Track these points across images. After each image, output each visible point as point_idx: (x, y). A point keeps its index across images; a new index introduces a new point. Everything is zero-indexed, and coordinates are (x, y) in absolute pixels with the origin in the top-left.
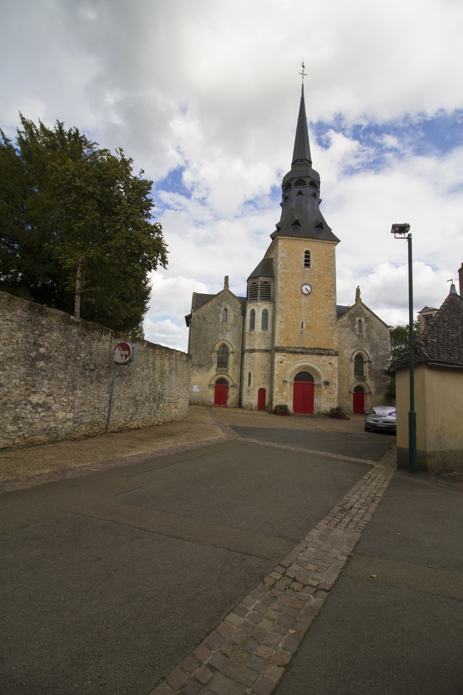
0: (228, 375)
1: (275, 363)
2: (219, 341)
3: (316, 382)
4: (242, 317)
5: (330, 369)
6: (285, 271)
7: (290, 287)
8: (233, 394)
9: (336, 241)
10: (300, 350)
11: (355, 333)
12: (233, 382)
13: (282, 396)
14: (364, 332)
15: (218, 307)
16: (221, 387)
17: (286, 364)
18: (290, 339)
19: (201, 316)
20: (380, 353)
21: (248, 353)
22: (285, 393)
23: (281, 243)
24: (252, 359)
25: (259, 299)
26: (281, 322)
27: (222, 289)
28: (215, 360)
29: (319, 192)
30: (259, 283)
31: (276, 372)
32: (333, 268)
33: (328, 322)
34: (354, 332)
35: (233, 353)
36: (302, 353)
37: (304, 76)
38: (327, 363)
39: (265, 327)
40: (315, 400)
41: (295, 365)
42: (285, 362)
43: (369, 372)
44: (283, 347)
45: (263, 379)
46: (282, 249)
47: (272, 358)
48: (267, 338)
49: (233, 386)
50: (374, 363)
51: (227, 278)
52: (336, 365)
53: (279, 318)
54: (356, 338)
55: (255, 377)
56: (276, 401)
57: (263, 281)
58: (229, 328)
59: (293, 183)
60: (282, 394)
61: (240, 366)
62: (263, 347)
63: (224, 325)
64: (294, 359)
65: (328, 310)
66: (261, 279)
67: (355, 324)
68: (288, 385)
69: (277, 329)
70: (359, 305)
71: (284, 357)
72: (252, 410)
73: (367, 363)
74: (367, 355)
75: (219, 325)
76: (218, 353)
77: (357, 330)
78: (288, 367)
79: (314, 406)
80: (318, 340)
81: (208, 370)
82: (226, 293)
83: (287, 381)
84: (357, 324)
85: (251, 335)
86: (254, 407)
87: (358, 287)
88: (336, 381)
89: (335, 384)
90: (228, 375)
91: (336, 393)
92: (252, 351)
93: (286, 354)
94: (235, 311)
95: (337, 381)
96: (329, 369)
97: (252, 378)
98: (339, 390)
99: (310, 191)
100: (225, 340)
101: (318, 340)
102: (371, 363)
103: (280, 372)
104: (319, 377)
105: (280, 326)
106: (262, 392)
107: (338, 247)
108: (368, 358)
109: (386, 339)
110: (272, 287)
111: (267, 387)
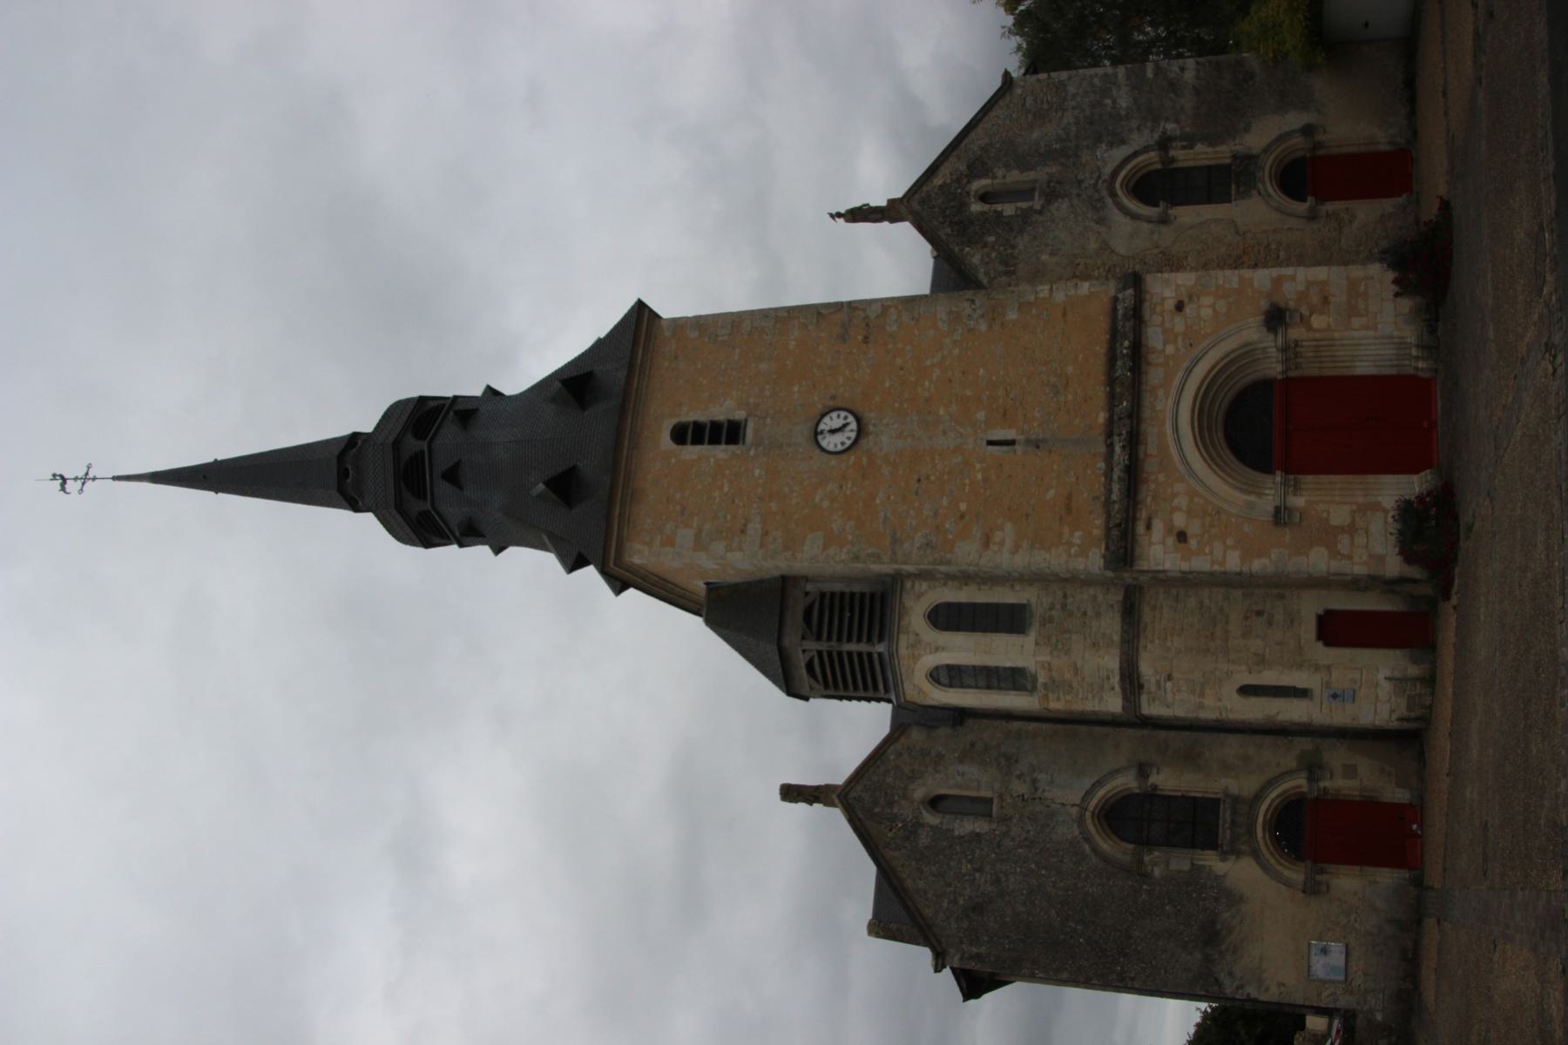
0: (1258, 797)
1: (1185, 566)
2: (1088, 839)
3: (1273, 367)
4: (970, 722)
5: (1205, 308)
6: (755, 527)
7: (826, 504)
8: (1350, 771)
9: (641, 311)
10: (1118, 449)
11: (1040, 212)
12: (1290, 773)
14: (1031, 175)
15: (924, 839)
16: (1317, 833)
17: (1190, 512)
18: (1069, 497)
19: (965, 924)
20: (1124, 103)
21: (1144, 698)
22: (1339, 515)
23: (639, 556)
24: (1169, 677)
26: (987, 542)
27: (836, 816)
28: (1180, 861)
29: (456, 398)
30: (813, 646)
31: (1233, 562)
32: (747, 325)
33: (983, 327)
34: (1035, 217)
35: (1143, 771)
36: (1134, 441)
37: (91, 475)
38: (1179, 324)
39: (1009, 620)
40: (1364, 368)
41: (1192, 473)
42: (1179, 520)
43: (1212, 140)
44: (1108, 529)
47: (1162, 580)
48: (1064, 606)
49: (1313, 768)
50: (1171, 127)
51: (791, 793)
52: (1185, 279)
53: (967, 553)
54: (1061, 208)
55: (1261, 661)
57: (805, 631)
58: (1020, 788)
59: (417, 506)
60: (1342, 529)
62: (1111, 624)
64: (1161, 477)
66: (792, 640)
67: (999, 214)
68: (1298, 501)
69: (1020, 561)
70: (915, 205)
71: (1158, 525)
72: (1430, 681)
73: (1172, 153)
74: (1135, 154)
77: (1024, 205)
78: (1206, 513)
79: (1394, 372)
80: (1070, 369)
81: (1233, 899)
82: (864, 800)
83: (1277, 510)
84: (999, 207)
85: (1053, 685)
86: (1413, 671)
88: (1262, 278)
89: (1278, 282)
90: (1258, 797)
91: (1321, 273)
92: (1131, 681)
93: (1143, 514)
95: (1266, 272)
96: (1206, 313)
97: (1270, 677)
98: (1301, 259)
99: (449, 434)
100: (1083, 809)
101: (1070, 369)
103: (1230, 542)
104: (1247, 354)
106: (1338, 630)
107: (667, 307)
108: (1146, 150)
109: (1061, 86)
110: (828, 587)
111: (1310, 607)
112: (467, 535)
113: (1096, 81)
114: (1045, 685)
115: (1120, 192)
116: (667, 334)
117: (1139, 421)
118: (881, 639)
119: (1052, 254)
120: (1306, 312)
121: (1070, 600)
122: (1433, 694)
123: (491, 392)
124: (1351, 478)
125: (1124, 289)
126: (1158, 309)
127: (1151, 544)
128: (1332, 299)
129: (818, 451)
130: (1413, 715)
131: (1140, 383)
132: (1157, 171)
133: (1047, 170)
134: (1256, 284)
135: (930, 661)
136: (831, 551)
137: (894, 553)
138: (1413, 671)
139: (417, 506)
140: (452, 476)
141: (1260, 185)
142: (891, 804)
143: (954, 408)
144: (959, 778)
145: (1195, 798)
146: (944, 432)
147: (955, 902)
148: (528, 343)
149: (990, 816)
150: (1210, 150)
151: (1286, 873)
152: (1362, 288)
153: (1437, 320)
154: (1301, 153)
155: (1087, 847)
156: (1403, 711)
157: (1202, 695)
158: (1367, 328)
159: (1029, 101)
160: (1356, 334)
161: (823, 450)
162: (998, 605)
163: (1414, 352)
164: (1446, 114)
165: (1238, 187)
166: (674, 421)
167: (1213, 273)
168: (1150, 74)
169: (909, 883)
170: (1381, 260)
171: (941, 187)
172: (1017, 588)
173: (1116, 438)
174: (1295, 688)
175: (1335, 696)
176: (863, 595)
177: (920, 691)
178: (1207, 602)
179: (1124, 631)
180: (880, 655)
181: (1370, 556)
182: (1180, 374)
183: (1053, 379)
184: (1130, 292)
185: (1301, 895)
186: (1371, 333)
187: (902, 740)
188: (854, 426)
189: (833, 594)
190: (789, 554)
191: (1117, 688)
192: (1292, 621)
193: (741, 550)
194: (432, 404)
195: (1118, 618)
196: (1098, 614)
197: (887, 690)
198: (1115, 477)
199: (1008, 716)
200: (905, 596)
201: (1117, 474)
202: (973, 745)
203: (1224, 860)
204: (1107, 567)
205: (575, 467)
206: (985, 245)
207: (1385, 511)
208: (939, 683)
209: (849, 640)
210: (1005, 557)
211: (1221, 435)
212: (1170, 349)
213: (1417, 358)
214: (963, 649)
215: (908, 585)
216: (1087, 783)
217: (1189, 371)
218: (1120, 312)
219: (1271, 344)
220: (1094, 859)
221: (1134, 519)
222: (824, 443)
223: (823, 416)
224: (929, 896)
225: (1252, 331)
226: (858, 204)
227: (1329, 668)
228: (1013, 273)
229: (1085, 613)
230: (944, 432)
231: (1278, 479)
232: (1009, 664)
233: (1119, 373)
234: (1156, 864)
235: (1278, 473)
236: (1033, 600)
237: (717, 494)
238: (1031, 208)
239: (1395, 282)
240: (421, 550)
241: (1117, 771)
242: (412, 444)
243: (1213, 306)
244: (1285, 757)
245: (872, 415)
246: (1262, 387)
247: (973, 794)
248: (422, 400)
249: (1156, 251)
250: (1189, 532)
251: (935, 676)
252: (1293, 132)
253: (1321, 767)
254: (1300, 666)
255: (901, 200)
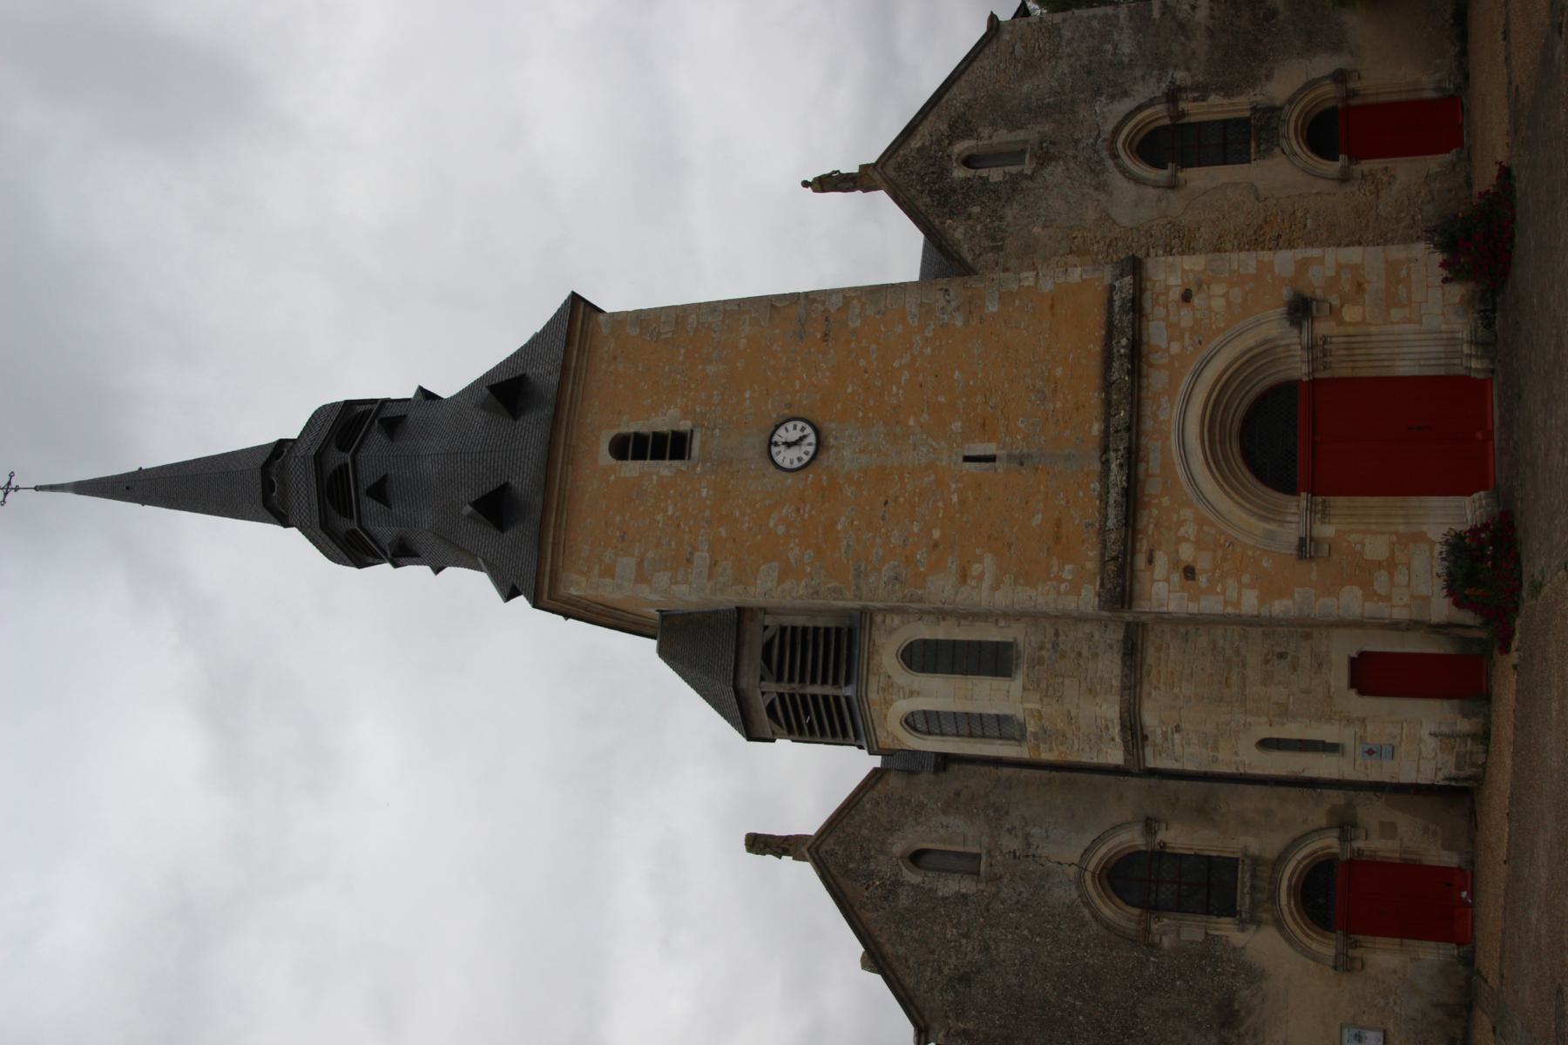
0: (1282, 859)
1: (1193, 608)
2: (1087, 904)
3: (1299, 369)
4: (955, 767)
5: (1216, 299)
6: (703, 556)
7: (781, 530)
8: (1389, 830)
9: (577, 309)
10: (1114, 467)
11: (1031, 178)
12: (1319, 830)
13: (1390, 565)
14: (1021, 135)
15: (904, 901)
16: (1351, 899)
17: (1199, 545)
18: (1059, 523)
19: (950, 996)
21: (1149, 751)
22: (1376, 549)
23: (576, 587)
24: (1178, 729)
25: (848, 691)
26: (964, 576)
27: (806, 870)
28: (1192, 930)
30: (773, 688)
31: (1250, 603)
32: (692, 319)
33: (959, 322)
34: (1025, 184)
36: (1133, 458)
37: (13, 485)
38: (1186, 317)
39: (992, 660)
42: (1187, 553)
43: (1228, 91)
44: (1104, 563)
45: (1294, 668)
46: (602, 575)
47: (1162, 618)
48: (1055, 645)
49: (1345, 825)
50: (1181, 76)
51: (758, 844)
53: (942, 588)
54: (1054, 172)
55: (1284, 712)
56: (1426, 600)
58: (1010, 843)
59: (345, 525)
61: (1224, 788)
62: (1110, 667)
63: (999, 870)
64: (1165, 501)
65: (899, 329)
66: (749, 679)
67: (985, 181)
68: (1327, 531)
69: (1001, 599)
70: (890, 171)
71: (1161, 559)
72: (1484, 737)
73: (1182, 106)
74: (1140, 108)
75: (995, 896)
76: (1152, 907)
77: (1013, 169)
78: (1218, 540)
79: (1442, 372)
80: (1059, 372)
81: (1255, 975)
82: (839, 854)
83: (1302, 541)
84: (984, 173)
85: (1044, 735)
86: (1464, 725)
87: (805, 184)
88: (1283, 261)
89: (1303, 266)
90: (1282, 859)
91: (1354, 254)
92: (1133, 731)
93: (1143, 546)
94: (921, 806)
96: (1218, 304)
101: (1059, 372)
102: (1180, 89)
103: (1246, 579)
105: (986, 584)
106: (1375, 675)
107: (612, 299)
108: (1152, 102)
110: (788, 621)
111: (1342, 649)
112: (401, 554)
113: (1095, 23)
114: (1035, 734)
115: (1122, 154)
116: (605, 331)
117: (1138, 435)
118: (848, 682)
119: (1045, 226)
120: (1336, 303)
121: (1062, 638)
122: (1487, 751)
123: (425, 395)
124: (1390, 500)
125: (1122, 276)
126: (1162, 299)
127: (1153, 581)
128: (1366, 285)
129: (772, 468)
130: (1463, 774)
131: (1140, 388)
132: (1165, 127)
133: (1039, 128)
134: (1277, 271)
135: (903, 706)
136: (787, 585)
137: (858, 587)
138: (1464, 725)
139: (345, 525)
140: (379, 491)
141: (1284, 143)
142: (867, 859)
143: (925, 417)
144: (942, 831)
145: (1209, 857)
146: (915, 447)
147: (940, 971)
148: (441, 349)
149: (978, 874)
150: (1226, 101)
151: (1314, 946)
152: (1404, 273)
153: (1494, 310)
154: (1332, 104)
155: (1086, 912)
156: (1450, 769)
157: (1215, 748)
158: (1410, 321)
159: (1018, 50)
160: (1397, 328)
161: (778, 466)
162: (980, 643)
163: (1466, 349)
164: (1507, 59)
165: (1258, 146)
166: (614, 432)
167: (1226, 256)
168: (1156, 14)
169: (888, 949)
170: (1431, 240)
171: (919, 150)
172: (1002, 623)
173: (1112, 454)
174: (1323, 742)
175: (1370, 752)
176: (827, 630)
177: (895, 738)
178: (1220, 643)
179: (1125, 676)
180: (847, 698)
181: (1412, 597)
182: (1187, 379)
183: (1039, 383)
184: (1128, 279)
185: (1332, 972)
186: (1417, 327)
187: (879, 787)
188: (812, 438)
189: (794, 629)
190: (740, 588)
191: (1118, 739)
192: (1320, 665)
193: (686, 582)
194: (361, 409)
195: (1118, 660)
196: (1095, 656)
197: (857, 736)
198: (1111, 501)
199: (998, 762)
200: (875, 633)
201: (1114, 496)
202: (958, 794)
203: (1242, 930)
204: (1101, 608)
205: (506, 484)
206: (970, 216)
207: (1432, 543)
208: (915, 729)
209: (813, 682)
210: (982, 595)
211: (1236, 448)
212: (1175, 348)
213: (1470, 356)
214: (940, 693)
215: (879, 619)
216: (1087, 839)
217: (1197, 375)
218: (1117, 304)
219: (1293, 339)
220: (1094, 925)
221: (1134, 552)
222: (778, 459)
223: (777, 427)
224: (911, 963)
225: (1272, 325)
226: (827, 171)
227: (1363, 721)
228: (1001, 248)
229: (1080, 654)
230: (915, 447)
231: (1304, 503)
232: (993, 711)
233: (1115, 376)
234: (1165, 933)
235: (1304, 495)
236: (1021, 638)
237: (659, 517)
238: (1021, 173)
239: (1442, 265)
240: (353, 570)
241: (1120, 826)
242: (337, 458)
243: (1225, 295)
244: (1312, 813)
245: (833, 425)
246: (1284, 392)
247: (961, 849)
248: (349, 405)
249: (1164, 221)
250: (1198, 567)
251: (910, 722)
252: (1324, 78)
253: (1354, 825)
254: (1330, 719)
255: (874, 166)
